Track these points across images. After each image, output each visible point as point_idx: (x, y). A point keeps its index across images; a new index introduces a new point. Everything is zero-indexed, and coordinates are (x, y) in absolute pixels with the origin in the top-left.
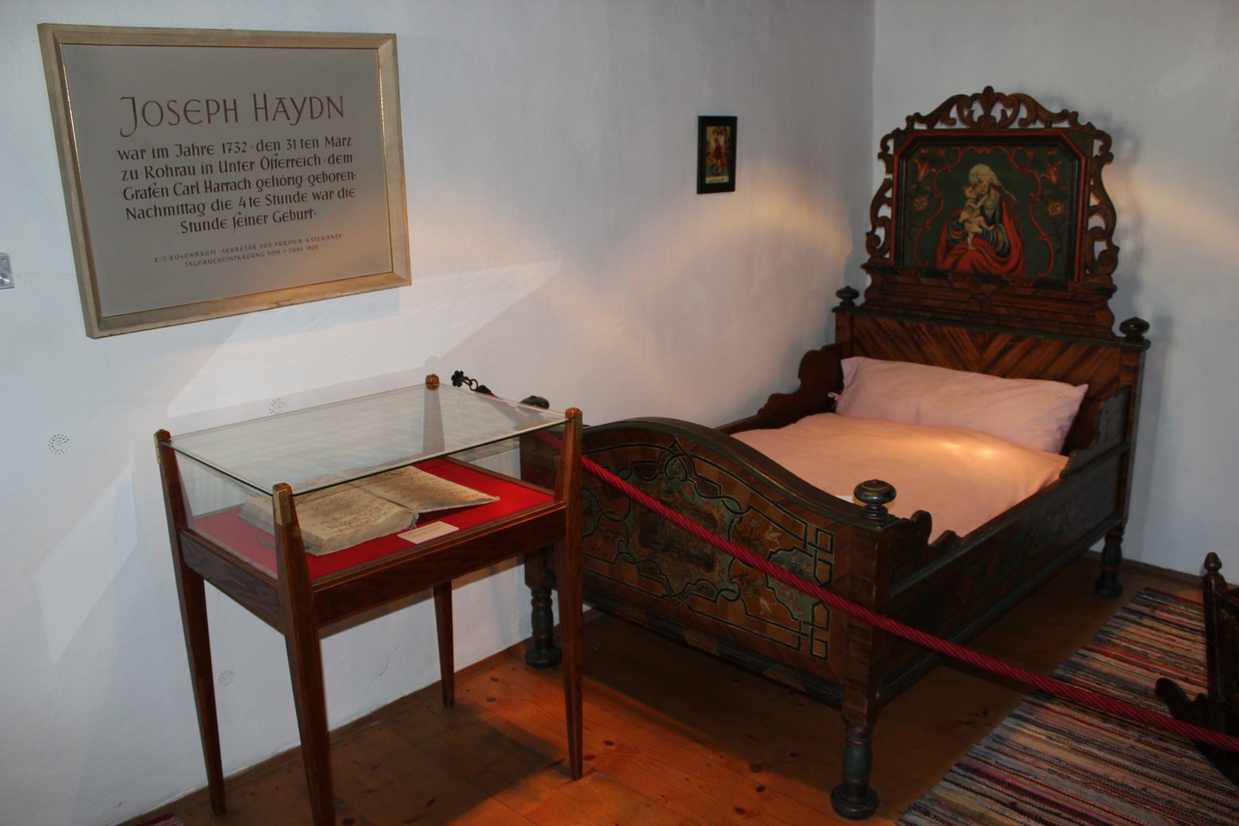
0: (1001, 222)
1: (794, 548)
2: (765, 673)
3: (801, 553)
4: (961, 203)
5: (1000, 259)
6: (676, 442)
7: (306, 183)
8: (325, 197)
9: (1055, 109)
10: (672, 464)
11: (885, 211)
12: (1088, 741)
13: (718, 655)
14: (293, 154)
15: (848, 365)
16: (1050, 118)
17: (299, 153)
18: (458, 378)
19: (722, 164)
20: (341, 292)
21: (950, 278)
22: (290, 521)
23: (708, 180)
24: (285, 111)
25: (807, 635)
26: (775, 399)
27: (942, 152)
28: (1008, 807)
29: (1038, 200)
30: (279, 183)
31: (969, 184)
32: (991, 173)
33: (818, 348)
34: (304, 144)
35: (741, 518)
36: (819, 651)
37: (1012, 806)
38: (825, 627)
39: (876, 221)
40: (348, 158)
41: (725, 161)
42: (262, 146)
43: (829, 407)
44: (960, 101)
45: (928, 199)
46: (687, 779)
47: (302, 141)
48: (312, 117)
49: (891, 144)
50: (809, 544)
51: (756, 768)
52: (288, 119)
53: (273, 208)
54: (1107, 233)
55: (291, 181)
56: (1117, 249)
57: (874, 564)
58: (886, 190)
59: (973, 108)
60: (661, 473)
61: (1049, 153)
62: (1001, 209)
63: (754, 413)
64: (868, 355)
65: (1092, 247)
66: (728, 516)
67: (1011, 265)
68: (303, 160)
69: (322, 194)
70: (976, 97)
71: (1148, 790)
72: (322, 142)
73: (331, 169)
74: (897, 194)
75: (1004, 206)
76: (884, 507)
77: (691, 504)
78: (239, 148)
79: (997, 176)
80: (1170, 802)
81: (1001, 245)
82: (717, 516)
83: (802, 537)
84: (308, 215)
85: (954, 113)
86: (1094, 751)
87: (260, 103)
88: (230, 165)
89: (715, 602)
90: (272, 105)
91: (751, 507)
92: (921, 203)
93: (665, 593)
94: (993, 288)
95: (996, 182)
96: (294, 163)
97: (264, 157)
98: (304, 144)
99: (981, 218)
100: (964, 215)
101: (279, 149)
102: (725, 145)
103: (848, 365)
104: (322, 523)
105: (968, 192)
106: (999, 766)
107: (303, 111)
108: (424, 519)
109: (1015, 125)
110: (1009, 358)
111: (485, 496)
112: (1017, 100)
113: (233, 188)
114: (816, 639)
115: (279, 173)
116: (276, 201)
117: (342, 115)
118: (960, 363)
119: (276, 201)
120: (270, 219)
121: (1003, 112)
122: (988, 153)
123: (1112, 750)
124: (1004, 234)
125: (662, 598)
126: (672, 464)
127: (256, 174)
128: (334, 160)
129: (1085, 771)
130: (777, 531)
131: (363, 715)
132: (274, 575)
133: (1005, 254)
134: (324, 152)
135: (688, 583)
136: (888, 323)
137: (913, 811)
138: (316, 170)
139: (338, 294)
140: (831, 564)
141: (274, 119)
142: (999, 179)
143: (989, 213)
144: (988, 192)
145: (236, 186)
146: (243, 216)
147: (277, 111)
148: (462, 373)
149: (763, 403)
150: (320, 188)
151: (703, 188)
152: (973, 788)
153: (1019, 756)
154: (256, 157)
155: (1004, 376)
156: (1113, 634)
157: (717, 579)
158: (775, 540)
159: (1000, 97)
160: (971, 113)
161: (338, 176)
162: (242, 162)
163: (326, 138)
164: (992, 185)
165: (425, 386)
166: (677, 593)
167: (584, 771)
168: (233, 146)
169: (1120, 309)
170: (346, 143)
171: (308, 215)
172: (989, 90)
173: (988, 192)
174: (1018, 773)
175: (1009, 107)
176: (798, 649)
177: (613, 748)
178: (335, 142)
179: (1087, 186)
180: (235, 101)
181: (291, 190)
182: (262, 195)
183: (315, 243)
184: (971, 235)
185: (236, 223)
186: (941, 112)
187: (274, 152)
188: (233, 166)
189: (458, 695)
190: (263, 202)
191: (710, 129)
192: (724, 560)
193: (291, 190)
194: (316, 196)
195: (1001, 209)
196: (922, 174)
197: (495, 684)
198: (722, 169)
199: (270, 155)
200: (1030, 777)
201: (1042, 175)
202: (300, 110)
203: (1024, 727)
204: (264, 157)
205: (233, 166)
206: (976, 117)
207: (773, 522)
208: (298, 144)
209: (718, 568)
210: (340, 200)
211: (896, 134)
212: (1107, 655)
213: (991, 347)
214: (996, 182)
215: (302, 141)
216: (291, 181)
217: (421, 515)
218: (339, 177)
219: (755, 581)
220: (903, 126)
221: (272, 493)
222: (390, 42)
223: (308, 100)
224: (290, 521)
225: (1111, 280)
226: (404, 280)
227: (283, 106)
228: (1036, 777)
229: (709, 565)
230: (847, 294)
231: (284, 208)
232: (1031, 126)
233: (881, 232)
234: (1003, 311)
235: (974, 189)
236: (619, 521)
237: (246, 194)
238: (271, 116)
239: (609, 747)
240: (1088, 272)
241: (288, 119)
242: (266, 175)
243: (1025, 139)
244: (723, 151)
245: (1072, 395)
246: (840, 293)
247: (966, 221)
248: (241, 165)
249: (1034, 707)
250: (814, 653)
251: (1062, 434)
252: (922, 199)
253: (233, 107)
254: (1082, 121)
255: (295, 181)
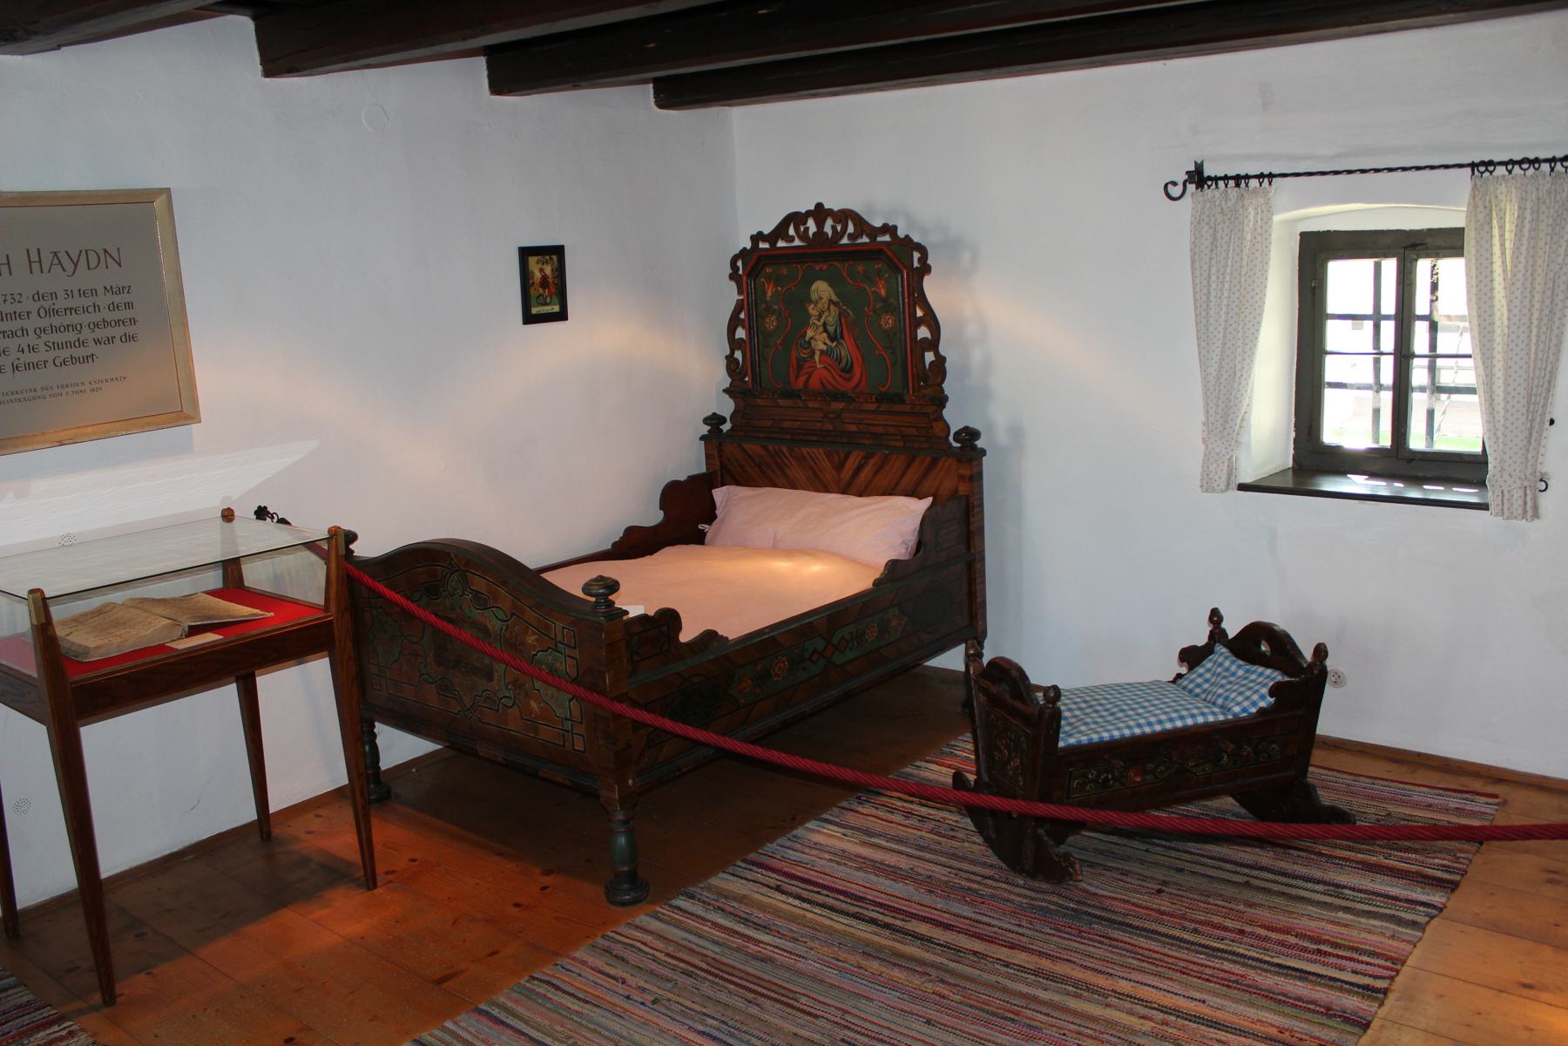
0: (842, 337)
1: (549, 648)
2: (540, 773)
3: (555, 653)
4: (805, 321)
5: (842, 374)
6: (452, 559)
7: (86, 330)
8: (107, 342)
9: (877, 223)
10: (452, 581)
11: (741, 333)
12: (881, 835)
13: (504, 762)
14: (71, 303)
15: (719, 494)
16: (874, 232)
17: (77, 302)
18: (262, 513)
19: (551, 294)
20: (126, 430)
21: (803, 398)
22: (44, 621)
23: (534, 311)
24: (60, 263)
25: (568, 731)
26: (630, 531)
27: (785, 270)
28: (774, 889)
29: (871, 313)
30: (58, 330)
31: (811, 302)
32: (830, 289)
33: (682, 477)
34: (82, 293)
35: (508, 626)
36: (579, 747)
37: (778, 889)
38: (580, 720)
39: (734, 343)
40: (129, 305)
41: (553, 290)
42: (38, 296)
43: (699, 539)
44: (796, 218)
45: (777, 319)
46: (477, 884)
47: (79, 290)
48: (89, 269)
49: (740, 264)
50: (559, 642)
51: (547, 872)
52: (64, 270)
53: (52, 354)
54: (933, 344)
55: (70, 328)
56: (944, 359)
57: (604, 653)
58: (740, 312)
59: (808, 225)
60: (444, 591)
61: (876, 267)
62: (841, 325)
63: (608, 546)
64: (738, 483)
65: (923, 357)
66: (498, 624)
67: (855, 380)
68: (81, 309)
69: (104, 339)
70: (809, 214)
71: (915, 869)
72: (101, 291)
73: (110, 316)
74: (749, 315)
75: (843, 321)
76: (610, 600)
77: (470, 617)
78: (15, 300)
79: (834, 290)
80: (930, 877)
81: (845, 361)
82: (490, 627)
83: (553, 636)
84: (90, 360)
85: (792, 231)
86: (884, 843)
87: (34, 257)
88: (6, 315)
89: (498, 710)
90: (47, 258)
91: (514, 614)
92: (771, 323)
93: (460, 709)
94: (842, 405)
95: (834, 298)
96: (73, 312)
97: (42, 307)
98: (82, 293)
99: (825, 335)
100: (810, 333)
101: (56, 298)
102: (553, 274)
103: (719, 494)
104: (95, 637)
105: (812, 310)
106: (783, 859)
107: (79, 264)
108: (194, 631)
109: (845, 241)
110: (863, 477)
111: (258, 611)
112: (844, 216)
113: (10, 336)
114: (576, 734)
115: (56, 321)
116: (56, 347)
117: (120, 265)
118: (820, 485)
119: (56, 347)
120: (50, 364)
121: (834, 228)
122: (824, 268)
123: (899, 841)
124: (845, 350)
125: (457, 714)
126: (452, 581)
127: (33, 323)
128: (114, 307)
129: (864, 858)
130: (535, 634)
131: (175, 849)
132: (35, 675)
133: (848, 370)
134: (103, 300)
135: (476, 695)
136: (753, 448)
137: (680, 897)
138: (96, 317)
139: (124, 433)
140: (576, 659)
141: (49, 272)
142: (836, 295)
143: (832, 329)
144: (829, 308)
145: (14, 334)
146: (22, 361)
147: (52, 264)
148: (265, 508)
149: (617, 535)
150: (102, 333)
151: (529, 319)
152: (748, 877)
153: (807, 850)
154: (34, 307)
155: (860, 495)
156: (958, 746)
157: (497, 688)
158: (534, 643)
159: (830, 213)
160: (807, 229)
161: (118, 323)
162: (18, 311)
163: (105, 288)
164: (831, 302)
165: (221, 518)
166: (469, 707)
167: (379, 884)
168: (9, 298)
169: (955, 417)
170: (126, 291)
171: (90, 360)
172: (819, 206)
173: (829, 308)
174: (797, 863)
175: (838, 223)
176: (564, 746)
177: (416, 863)
178: (114, 290)
179: (911, 298)
180: (7, 256)
181: (71, 336)
182: (41, 342)
183: (98, 385)
184: (818, 353)
185: (15, 368)
186: (780, 231)
187: (50, 302)
188: (9, 316)
189: (276, 832)
190: (42, 348)
191: (533, 260)
192: (500, 668)
193: (71, 336)
194: (97, 342)
195: (841, 325)
196: (769, 294)
197: (317, 820)
198: (551, 298)
199: (47, 305)
200: (808, 866)
201: (873, 289)
202: (75, 261)
203: (824, 828)
204: (42, 307)
205: (9, 316)
206: (811, 233)
207: (532, 626)
208: (76, 293)
209: (496, 677)
210: (124, 344)
211: (743, 253)
212: (942, 765)
213: (847, 465)
214: (834, 298)
215: (79, 290)
216: (70, 328)
217: (190, 627)
218: (121, 323)
219: (524, 685)
220: (749, 246)
221: (26, 597)
222: (164, 196)
223: (84, 253)
224: (44, 621)
225: (943, 391)
226: (192, 418)
227: (58, 258)
228: (813, 866)
229: (489, 676)
230: (714, 421)
231: (65, 353)
232: (860, 241)
233: (738, 355)
234: (854, 428)
235: (816, 305)
236: (417, 643)
237: (24, 342)
238: (45, 270)
239: (412, 863)
240: (922, 384)
241: (64, 270)
242: (45, 323)
243: (855, 254)
244: (550, 280)
245: (920, 506)
246: (706, 421)
247: (812, 338)
248: (17, 314)
249: (843, 811)
250: (576, 748)
251: (907, 549)
252: (772, 319)
253: (37, 259)
254: (901, 234)
255: (74, 328)
